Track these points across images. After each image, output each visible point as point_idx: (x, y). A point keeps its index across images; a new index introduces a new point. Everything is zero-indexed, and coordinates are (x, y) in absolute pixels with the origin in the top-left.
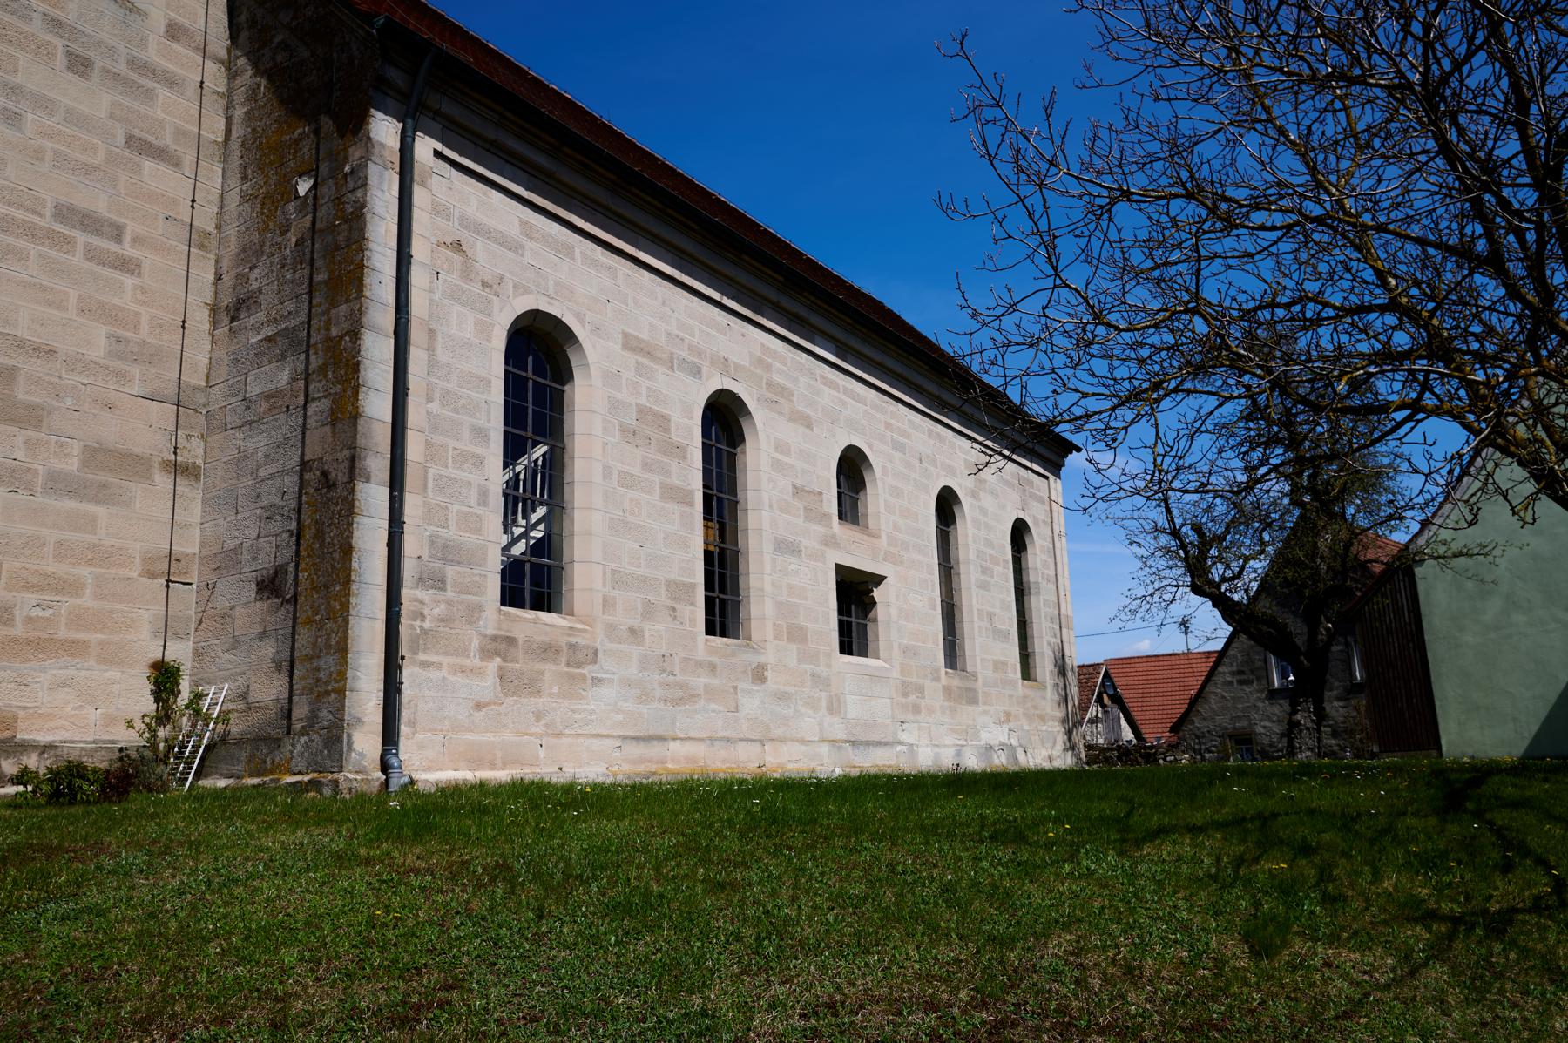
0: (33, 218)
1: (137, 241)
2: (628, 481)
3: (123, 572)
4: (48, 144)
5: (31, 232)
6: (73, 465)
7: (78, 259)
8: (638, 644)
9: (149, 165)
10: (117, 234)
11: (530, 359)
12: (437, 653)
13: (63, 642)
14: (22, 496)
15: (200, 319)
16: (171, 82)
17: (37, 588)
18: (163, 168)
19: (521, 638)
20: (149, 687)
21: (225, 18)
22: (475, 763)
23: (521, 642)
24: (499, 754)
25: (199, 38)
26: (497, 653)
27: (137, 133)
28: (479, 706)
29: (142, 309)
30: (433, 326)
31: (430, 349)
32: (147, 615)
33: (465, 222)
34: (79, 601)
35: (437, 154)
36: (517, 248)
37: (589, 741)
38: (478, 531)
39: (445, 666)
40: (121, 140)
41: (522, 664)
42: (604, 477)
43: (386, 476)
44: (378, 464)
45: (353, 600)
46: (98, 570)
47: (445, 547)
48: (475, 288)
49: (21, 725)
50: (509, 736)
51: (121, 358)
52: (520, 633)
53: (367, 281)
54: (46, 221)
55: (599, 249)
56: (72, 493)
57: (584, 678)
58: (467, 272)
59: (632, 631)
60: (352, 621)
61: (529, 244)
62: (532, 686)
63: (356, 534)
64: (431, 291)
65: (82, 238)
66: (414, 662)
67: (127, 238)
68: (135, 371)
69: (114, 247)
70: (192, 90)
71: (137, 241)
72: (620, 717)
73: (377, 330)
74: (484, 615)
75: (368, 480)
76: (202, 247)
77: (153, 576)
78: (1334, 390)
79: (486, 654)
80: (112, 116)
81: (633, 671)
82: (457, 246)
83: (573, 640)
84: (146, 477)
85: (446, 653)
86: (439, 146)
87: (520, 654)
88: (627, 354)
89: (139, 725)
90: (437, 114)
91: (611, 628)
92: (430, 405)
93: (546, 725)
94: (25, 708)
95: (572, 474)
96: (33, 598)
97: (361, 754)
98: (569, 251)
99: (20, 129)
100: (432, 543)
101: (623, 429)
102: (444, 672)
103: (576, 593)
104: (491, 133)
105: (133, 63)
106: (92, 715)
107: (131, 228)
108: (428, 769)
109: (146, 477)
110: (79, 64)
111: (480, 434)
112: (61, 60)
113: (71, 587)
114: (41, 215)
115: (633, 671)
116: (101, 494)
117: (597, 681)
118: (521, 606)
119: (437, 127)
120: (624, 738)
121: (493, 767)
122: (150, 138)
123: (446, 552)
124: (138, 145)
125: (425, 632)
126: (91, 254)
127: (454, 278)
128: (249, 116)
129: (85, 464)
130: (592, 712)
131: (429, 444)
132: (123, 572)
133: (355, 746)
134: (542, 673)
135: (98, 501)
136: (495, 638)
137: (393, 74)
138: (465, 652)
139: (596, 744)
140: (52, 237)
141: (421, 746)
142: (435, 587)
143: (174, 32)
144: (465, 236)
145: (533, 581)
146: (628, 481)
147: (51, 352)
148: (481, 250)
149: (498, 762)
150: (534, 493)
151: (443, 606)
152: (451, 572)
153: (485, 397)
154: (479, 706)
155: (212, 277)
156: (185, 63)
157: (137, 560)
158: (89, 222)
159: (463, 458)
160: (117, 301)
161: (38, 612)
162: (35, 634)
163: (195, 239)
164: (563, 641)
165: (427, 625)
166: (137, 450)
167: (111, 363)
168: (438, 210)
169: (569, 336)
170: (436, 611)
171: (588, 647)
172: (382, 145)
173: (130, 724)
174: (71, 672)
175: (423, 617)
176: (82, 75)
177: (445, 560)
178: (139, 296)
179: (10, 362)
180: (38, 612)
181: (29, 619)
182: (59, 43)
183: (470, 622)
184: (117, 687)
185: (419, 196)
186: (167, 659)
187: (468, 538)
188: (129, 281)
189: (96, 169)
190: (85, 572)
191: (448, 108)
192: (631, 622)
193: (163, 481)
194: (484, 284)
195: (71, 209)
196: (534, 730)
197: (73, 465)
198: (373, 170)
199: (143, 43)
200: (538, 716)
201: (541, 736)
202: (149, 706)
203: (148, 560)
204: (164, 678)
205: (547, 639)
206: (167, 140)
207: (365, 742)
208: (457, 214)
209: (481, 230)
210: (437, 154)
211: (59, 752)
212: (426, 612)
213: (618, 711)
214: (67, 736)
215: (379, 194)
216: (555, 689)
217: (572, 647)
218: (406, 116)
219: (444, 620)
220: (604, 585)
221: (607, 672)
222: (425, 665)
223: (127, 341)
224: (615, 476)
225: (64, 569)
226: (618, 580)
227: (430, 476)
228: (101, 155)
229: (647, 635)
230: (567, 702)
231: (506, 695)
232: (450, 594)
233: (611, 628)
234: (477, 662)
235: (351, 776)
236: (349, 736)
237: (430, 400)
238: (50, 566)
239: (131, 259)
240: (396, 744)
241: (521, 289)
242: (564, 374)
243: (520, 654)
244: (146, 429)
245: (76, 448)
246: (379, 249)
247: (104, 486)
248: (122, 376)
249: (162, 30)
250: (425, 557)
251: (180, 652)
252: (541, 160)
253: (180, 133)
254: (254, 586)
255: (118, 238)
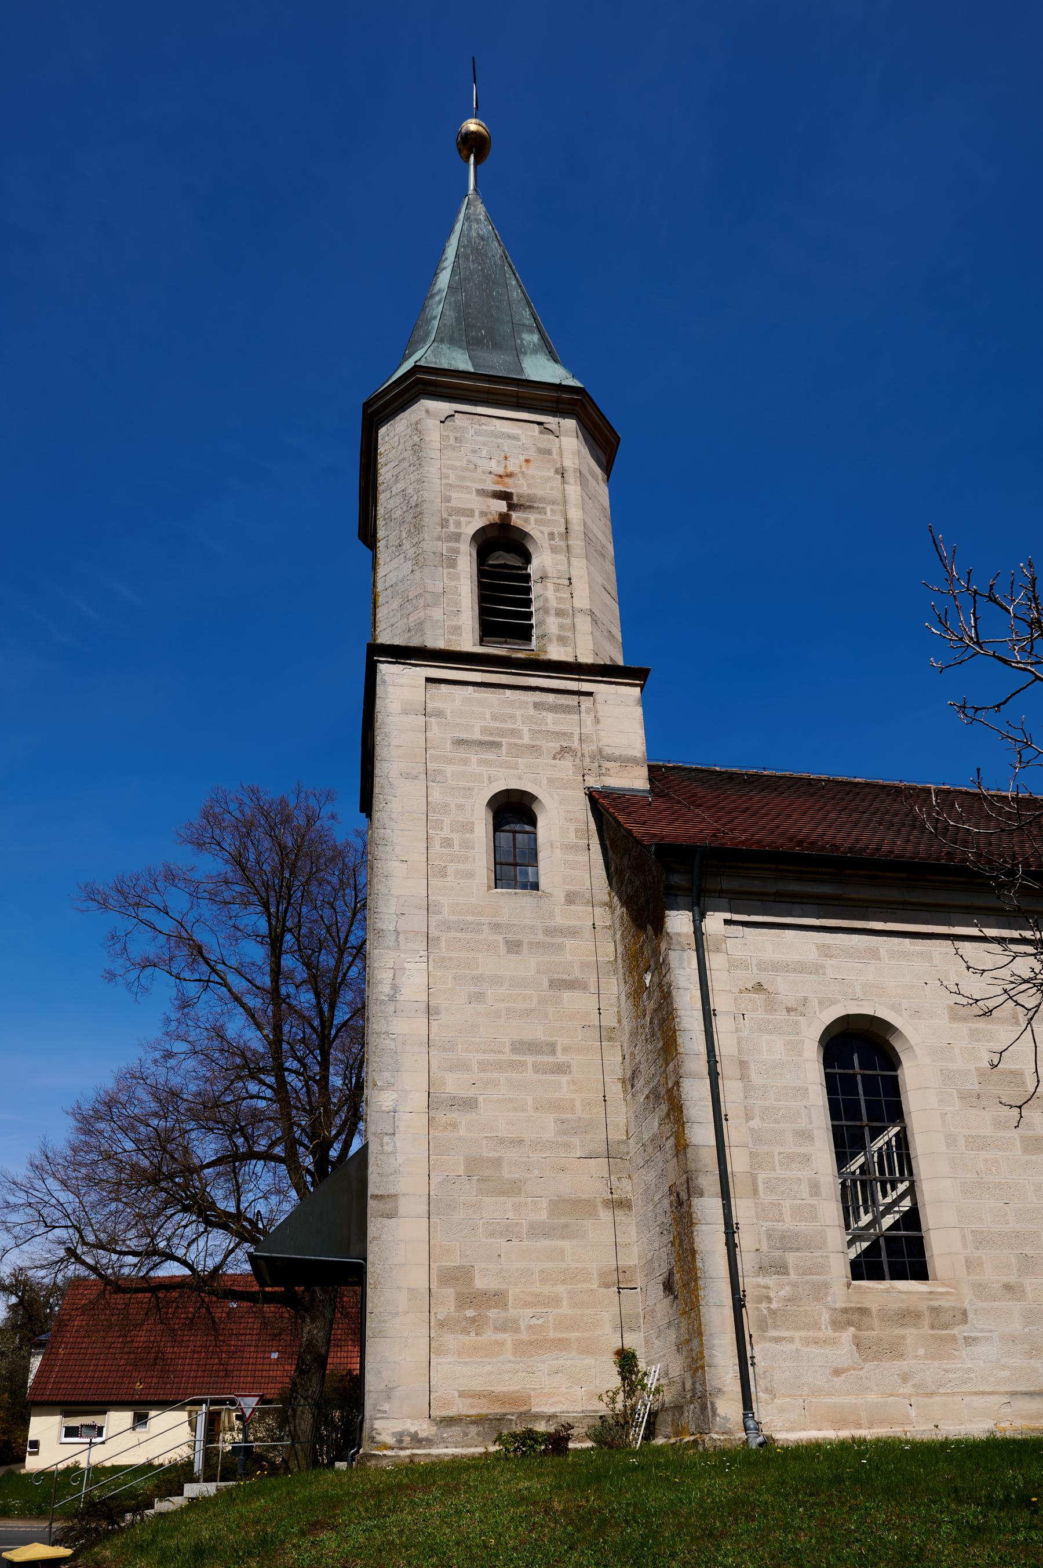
0: (500, 1057)
1: (566, 1050)
2: (977, 1143)
3: (587, 1286)
4: (502, 1005)
5: (499, 1066)
6: (543, 1215)
7: (530, 1075)
8: (1018, 1300)
9: (566, 995)
10: (552, 1049)
11: (855, 1057)
12: (788, 1329)
13: (553, 1340)
14: (515, 1243)
15: (616, 1091)
16: (573, 933)
17: (533, 1305)
18: (576, 994)
19: (874, 1307)
20: (616, 1369)
21: (604, 873)
22: (839, 1423)
23: (874, 1312)
24: (863, 1414)
25: (588, 895)
26: (850, 1323)
27: (556, 976)
28: (837, 1372)
29: (575, 1096)
30: (745, 1058)
31: (743, 1077)
32: (607, 1318)
33: (762, 966)
34: (559, 1311)
35: (727, 922)
36: (816, 969)
37: (967, 1399)
38: (814, 1218)
39: (797, 1340)
40: (546, 985)
41: (877, 1331)
42: (948, 1146)
43: (718, 1189)
44: (709, 1182)
45: (701, 1293)
46: (569, 1287)
47: (783, 1237)
48: (782, 1016)
49: (533, 1402)
50: (872, 1398)
51: (565, 1134)
52: (872, 1303)
53: (680, 1041)
54: (508, 1056)
55: (907, 941)
56: (546, 1235)
57: (954, 1339)
58: (770, 1006)
59: (1008, 1287)
60: (703, 1310)
61: (829, 962)
62: (894, 1351)
63: (697, 1240)
64: (737, 1030)
65: (529, 1059)
66: (764, 1339)
67: (559, 1050)
68: (576, 1140)
69: (550, 1059)
70: (588, 932)
71: (566, 1050)
72: (1007, 1373)
73: (691, 1075)
74: (831, 1291)
75: (701, 1195)
76: (610, 1039)
77: (608, 1286)
78: (17, 1296)
79: (838, 1325)
80: (538, 972)
81: (1016, 1327)
82: (759, 987)
83: (935, 1304)
84: (594, 1214)
85: (796, 1328)
86: (728, 916)
87: (876, 1322)
88: (955, 1025)
89: (606, 1399)
90: (721, 893)
91: (981, 1290)
92: (751, 1123)
93: (915, 1386)
94: (534, 1389)
95: (915, 1149)
96: (530, 1312)
97: (725, 1418)
98: (874, 954)
99: (485, 1003)
100: (769, 1236)
101: (963, 1096)
102: (797, 1344)
103: (936, 1258)
104: (772, 888)
105: (547, 932)
106: (579, 1392)
107: (561, 1042)
108: (792, 1430)
109: (594, 1214)
110: (514, 946)
111: (805, 1136)
112: (503, 948)
113: (554, 1301)
114: (503, 1053)
115: (1016, 1327)
116: (565, 1232)
117: (969, 1341)
118: (882, 1278)
119: (724, 901)
120: (1014, 1394)
121: (859, 1426)
122: (565, 977)
123: (785, 1242)
124: (560, 984)
125: (773, 1312)
126: (538, 1069)
127: (760, 1014)
128: (623, 937)
129: (552, 1213)
130: (970, 1370)
131: (753, 1155)
132: (587, 1286)
133: (718, 1411)
134: (904, 1337)
135: (563, 1238)
136: (845, 1311)
137: (677, 879)
138: (816, 1326)
139: (978, 1402)
140: (513, 1065)
141: (782, 1410)
142: (778, 1273)
143: (571, 898)
144: (764, 978)
145: (896, 1253)
146: (977, 1143)
147: (521, 1141)
148: (783, 986)
149: (864, 1421)
150: (892, 1172)
151: (787, 1288)
152: (791, 1258)
153: (804, 1103)
154: (837, 1372)
155: (620, 1059)
156: (581, 916)
157: (595, 1276)
158: (533, 1047)
159: (789, 1160)
160: (558, 1095)
161: (534, 1321)
162: (535, 1337)
163: (606, 1035)
164: (923, 1306)
165: (774, 1306)
166: (585, 1197)
167: (559, 1139)
168: (734, 965)
169: (888, 1027)
170: (782, 1293)
171: (954, 1308)
172: (679, 934)
173: (600, 1397)
174: (561, 1362)
175: (769, 1299)
176: (517, 953)
177: (785, 1249)
178: (572, 1087)
179: (497, 1155)
180: (534, 1321)
181: (530, 1327)
182: (500, 938)
183: (817, 1299)
184: (593, 1370)
185: (713, 961)
186: (625, 1347)
187: (804, 1227)
188: (564, 1079)
189: (533, 1010)
190: (561, 1289)
191: (727, 884)
192: (1005, 1279)
193: (605, 1215)
194: (789, 1010)
195: (521, 1042)
196: (901, 1391)
197: (543, 1215)
198: (674, 957)
199: (552, 915)
200: (905, 1378)
201: (910, 1396)
202: (616, 1381)
203: (602, 1275)
204: (626, 1361)
205: (904, 1306)
206: (577, 973)
207: (728, 1408)
208: (754, 962)
209: (778, 967)
210: (727, 922)
211: (559, 1420)
212: (772, 1295)
213: (1004, 1367)
214: (564, 1408)
215: (681, 972)
216: (921, 1352)
217: (936, 1311)
218: (693, 906)
219: (790, 1300)
220: (965, 1246)
221: (981, 1331)
222: (777, 1340)
223: (568, 1120)
224: (961, 1142)
225: (546, 1289)
226: (981, 1240)
227: (760, 1181)
228: (535, 999)
229: (1028, 1289)
230: (936, 1363)
231: (865, 1360)
232: (793, 1276)
233: (981, 1290)
234: (830, 1333)
235: (715, 1436)
236: (712, 1404)
237: (748, 1118)
238: (538, 1288)
239: (563, 1063)
240: (751, 1408)
241: (825, 1003)
242: (892, 1061)
243: (876, 1322)
244: (589, 1180)
245: (544, 1203)
246: (687, 1013)
247: (566, 1226)
248: (568, 1146)
249: (563, 900)
250: (764, 1247)
251: (633, 1341)
252: (827, 889)
253: (584, 965)
254: (661, 1287)
255: (553, 1052)
